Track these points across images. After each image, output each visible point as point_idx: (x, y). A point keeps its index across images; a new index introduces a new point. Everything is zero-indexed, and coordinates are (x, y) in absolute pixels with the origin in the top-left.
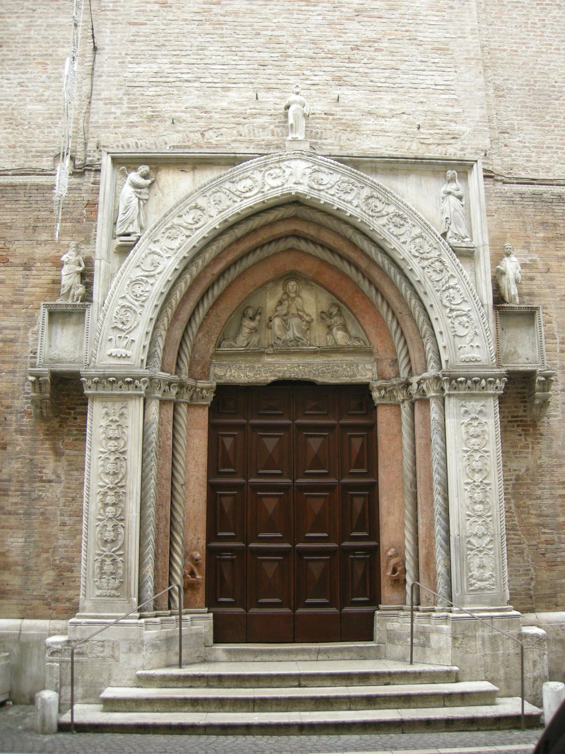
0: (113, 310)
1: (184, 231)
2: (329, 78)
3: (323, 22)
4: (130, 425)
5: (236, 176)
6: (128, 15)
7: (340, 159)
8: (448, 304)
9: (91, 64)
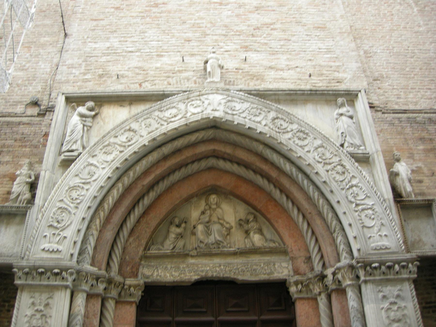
0: (51, 211)
1: (118, 147)
2: (237, 47)
3: (232, 14)
4: (53, 315)
5: (164, 107)
6: (91, 15)
7: (249, 92)
8: (353, 200)
9: (62, 45)
